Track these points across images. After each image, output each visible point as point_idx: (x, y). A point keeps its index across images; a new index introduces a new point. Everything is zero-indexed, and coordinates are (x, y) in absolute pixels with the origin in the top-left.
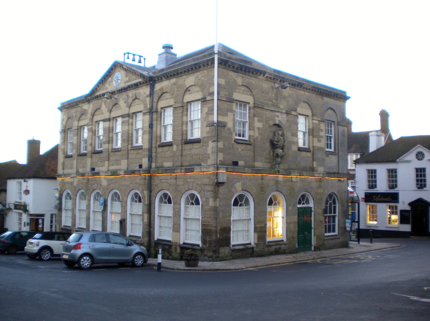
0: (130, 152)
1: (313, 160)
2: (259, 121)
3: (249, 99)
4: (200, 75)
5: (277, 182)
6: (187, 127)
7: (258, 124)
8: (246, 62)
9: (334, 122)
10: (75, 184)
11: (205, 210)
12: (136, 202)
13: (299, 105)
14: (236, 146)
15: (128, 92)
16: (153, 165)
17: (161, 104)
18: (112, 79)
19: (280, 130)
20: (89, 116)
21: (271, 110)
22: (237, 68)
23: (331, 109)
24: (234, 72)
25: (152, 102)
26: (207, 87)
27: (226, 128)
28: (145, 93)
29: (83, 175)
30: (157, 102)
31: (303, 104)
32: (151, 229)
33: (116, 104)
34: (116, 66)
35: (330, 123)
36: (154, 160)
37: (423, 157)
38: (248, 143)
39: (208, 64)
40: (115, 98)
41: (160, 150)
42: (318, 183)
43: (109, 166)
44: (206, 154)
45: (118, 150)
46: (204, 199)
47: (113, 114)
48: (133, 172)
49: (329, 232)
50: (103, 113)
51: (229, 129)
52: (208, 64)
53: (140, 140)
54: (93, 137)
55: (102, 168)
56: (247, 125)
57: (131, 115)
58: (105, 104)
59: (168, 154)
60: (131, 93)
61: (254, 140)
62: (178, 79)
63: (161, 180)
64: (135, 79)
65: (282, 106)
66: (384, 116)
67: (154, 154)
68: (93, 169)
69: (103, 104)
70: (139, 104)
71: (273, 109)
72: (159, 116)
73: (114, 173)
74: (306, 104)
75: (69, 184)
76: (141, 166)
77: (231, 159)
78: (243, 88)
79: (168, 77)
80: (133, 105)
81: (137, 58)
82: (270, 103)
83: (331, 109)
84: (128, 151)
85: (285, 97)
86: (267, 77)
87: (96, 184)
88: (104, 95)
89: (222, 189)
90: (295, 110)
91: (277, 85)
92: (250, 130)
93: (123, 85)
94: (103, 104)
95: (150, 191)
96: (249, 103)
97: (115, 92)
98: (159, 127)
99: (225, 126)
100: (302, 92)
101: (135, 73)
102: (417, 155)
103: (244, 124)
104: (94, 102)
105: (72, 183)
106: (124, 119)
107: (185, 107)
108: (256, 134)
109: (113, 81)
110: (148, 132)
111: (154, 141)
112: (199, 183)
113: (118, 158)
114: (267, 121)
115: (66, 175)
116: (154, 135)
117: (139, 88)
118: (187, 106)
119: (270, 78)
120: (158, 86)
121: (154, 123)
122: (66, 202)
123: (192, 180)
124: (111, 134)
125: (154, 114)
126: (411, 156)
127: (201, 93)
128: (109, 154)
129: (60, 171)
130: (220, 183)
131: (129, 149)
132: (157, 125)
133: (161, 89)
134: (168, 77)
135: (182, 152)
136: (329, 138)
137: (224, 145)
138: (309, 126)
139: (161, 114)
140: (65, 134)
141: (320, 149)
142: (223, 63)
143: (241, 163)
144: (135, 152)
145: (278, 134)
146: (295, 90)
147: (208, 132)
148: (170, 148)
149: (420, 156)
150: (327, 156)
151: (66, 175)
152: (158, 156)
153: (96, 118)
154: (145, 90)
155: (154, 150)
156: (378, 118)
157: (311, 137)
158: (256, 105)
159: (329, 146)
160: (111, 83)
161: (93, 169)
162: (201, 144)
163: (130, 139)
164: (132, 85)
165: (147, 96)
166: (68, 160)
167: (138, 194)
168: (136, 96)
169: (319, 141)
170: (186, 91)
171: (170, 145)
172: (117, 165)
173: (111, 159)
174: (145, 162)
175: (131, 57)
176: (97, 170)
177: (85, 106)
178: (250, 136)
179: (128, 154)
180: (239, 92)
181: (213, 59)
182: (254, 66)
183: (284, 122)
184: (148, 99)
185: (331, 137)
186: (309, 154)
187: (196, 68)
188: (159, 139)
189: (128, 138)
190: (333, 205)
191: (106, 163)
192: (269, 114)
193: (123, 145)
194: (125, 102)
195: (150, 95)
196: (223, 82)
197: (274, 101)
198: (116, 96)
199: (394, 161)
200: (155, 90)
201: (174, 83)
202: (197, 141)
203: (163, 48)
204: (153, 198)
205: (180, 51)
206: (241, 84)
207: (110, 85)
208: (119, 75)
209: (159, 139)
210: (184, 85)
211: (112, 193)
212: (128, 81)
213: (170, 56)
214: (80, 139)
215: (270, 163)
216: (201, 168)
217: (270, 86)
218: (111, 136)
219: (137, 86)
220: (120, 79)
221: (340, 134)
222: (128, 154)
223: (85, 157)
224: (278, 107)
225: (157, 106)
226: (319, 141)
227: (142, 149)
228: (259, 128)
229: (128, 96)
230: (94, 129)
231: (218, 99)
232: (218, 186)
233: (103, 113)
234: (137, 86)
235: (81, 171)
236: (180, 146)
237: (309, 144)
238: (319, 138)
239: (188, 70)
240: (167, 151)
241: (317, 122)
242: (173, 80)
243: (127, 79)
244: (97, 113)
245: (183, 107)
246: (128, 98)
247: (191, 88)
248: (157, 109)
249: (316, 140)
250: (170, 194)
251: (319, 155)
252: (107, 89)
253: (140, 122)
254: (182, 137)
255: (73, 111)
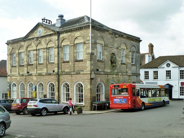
0: (48, 65)
1: (127, 68)
2: (106, 52)
3: (103, 42)
4: (83, 32)
5: (113, 78)
6: (76, 54)
7: (106, 53)
8: (101, 26)
9: (135, 52)
10: (18, 79)
11: (86, 90)
12: (14, 86)
13: (122, 45)
14: (98, 63)
15: (46, 38)
16: (60, 71)
17: (63, 44)
18: (37, 31)
19: (115, 56)
20: (25, 48)
21: (111, 47)
22: (98, 29)
23: (134, 46)
24: (97, 31)
25: (58, 43)
26: (86, 37)
27: (94, 55)
28: (55, 39)
29: (23, 75)
30: (61, 43)
31: (123, 44)
32: (60, 99)
33: (40, 43)
34: (38, 25)
35: (133, 52)
36: (60, 69)
37: (170, 66)
38: (102, 61)
39: (86, 28)
40: (39, 40)
41: (63, 64)
42: (129, 78)
43: (37, 71)
44: (86, 66)
45: (42, 64)
46: (85, 85)
47: (38, 48)
48: (50, 74)
49: (80, 102)
50: (33, 47)
51: (95, 56)
52: (86, 28)
53: (54, 60)
54: (28, 58)
55: (33, 72)
56: (102, 53)
57: (48, 48)
58: (34, 43)
59: (67, 66)
60: (48, 38)
61: (105, 60)
62: (71, 33)
63: (64, 77)
64: (50, 32)
65: (115, 45)
66: (61, 17)
67: (60, 66)
68: (28, 72)
69: (33, 43)
70: (52, 44)
71: (111, 47)
72: (62, 49)
73: (40, 75)
74: (124, 44)
75: (91, 82)
76: (54, 71)
77: (96, 68)
78: (100, 38)
79: (66, 32)
80: (48, 44)
81: (48, 21)
82: (110, 44)
83: (134, 46)
84: (47, 64)
85: (116, 41)
86: (110, 33)
87: (30, 79)
88: (33, 38)
89: (93, 81)
90: (120, 47)
91: (113, 36)
92: (103, 56)
93: (43, 35)
94: (33, 43)
95: (59, 82)
96: (102, 44)
97: (39, 37)
98: (62, 54)
99: (93, 54)
100: (123, 39)
101: (50, 29)
102: (167, 65)
103: (123, 57)
104: (27, 42)
105: (16, 79)
106: (44, 50)
107: (75, 46)
108: (105, 57)
109: (37, 32)
110: (57, 56)
111: (60, 60)
112: (83, 78)
113: (42, 68)
114: (109, 52)
115: (13, 76)
116: (60, 58)
117: (52, 36)
118: (76, 45)
119: (111, 33)
120: (61, 36)
121: (60, 52)
122: (13, 87)
123: (79, 77)
124: (37, 56)
125: (60, 48)
126: (165, 65)
127: (83, 40)
128: (37, 66)
129: (9, 72)
130: (92, 78)
131: (48, 64)
132: (61, 53)
133: (63, 37)
134: (66, 32)
135: (74, 65)
136: (132, 59)
137: (93, 63)
138: (125, 53)
139: (63, 48)
140: (11, 56)
141: (129, 63)
142: (93, 27)
143: (99, 70)
144: (51, 65)
145: (114, 57)
146: (120, 38)
147: (86, 57)
148: (68, 63)
149: (168, 65)
150: (132, 66)
151: (13, 76)
152: (62, 67)
153: (29, 49)
154: (56, 37)
155: (60, 64)
156: (148, 48)
157: (126, 58)
158: (105, 45)
159: (132, 62)
160: (37, 33)
161: (28, 72)
162: (83, 62)
163: (48, 59)
164: (48, 35)
165: (56, 40)
166: (13, 69)
167: (80, 84)
168: (50, 40)
169: (129, 60)
170: (75, 39)
171: (68, 62)
172: (41, 70)
173: (38, 68)
174: (56, 70)
175: (45, 21)
176: (30, 73)
177: (23, 43)
178: (103, 58)
179: (47, 66)
180: (99, 40)
181: (89, 25)
182: (104, 28)
183: (116, 52)
184: (57, 42)
185: (133, 58)
186: (125, 66)
187: (80, 29)
188: (62, 59)
189: (47, 59)
190: (53, 87)
191: (36, 70)
192: (110, 49)
193: (44, 61)
194: (45, 42)
195: (58, 39)
196: (93, 35)
197: (112, 43)
198: (40, 39)
199: (157, 68)
200: (60, 37)
201: (70, 35)
202: (82, 61)
203: (59, 17)
204: (60, 85)
205: (67, 18)
206: (99, 36)
207: (36, 34)
208: (41, 30)
209: (62, 59)
210: (75, 36)
211: (39, 83)
212: (46, 33)
213: (62, 21)
214: (20, 58)
215: (111, 69)
216: (83, 73)
217: (110, 37)
218: (37, 57)
219: (51, 35)
220: (41, 31)
221: (137, 57)
222: (47, 66)
223: (23, 67)
224: (114, 46)
225: (61, 45)
226: (129, 60)
227: (54, 63)
228: (106, 55)
229: (46, 39)
230: (28, 54)
231: (91, 43)
232: (92, 80)
233: (33, 47)
234: (51, 35)
235: (21, 73)
236: (73, 63)
237: (125, 61)
238: (129, 58)
239: (77, 30)
240: (67, 65)
241: (128, 52)
242: (69, 34)
243: (45, 32)
244: (29, 47)
245: (74, 46)
246: (46, 41)
247: (78, 38)
248: (61, 46)
249: (128, 59)
250: (53, 83)
251: (129, 66)
252: (34, 36)
253: (54, 52)
254: (74, 59)
255: (15, 45)
